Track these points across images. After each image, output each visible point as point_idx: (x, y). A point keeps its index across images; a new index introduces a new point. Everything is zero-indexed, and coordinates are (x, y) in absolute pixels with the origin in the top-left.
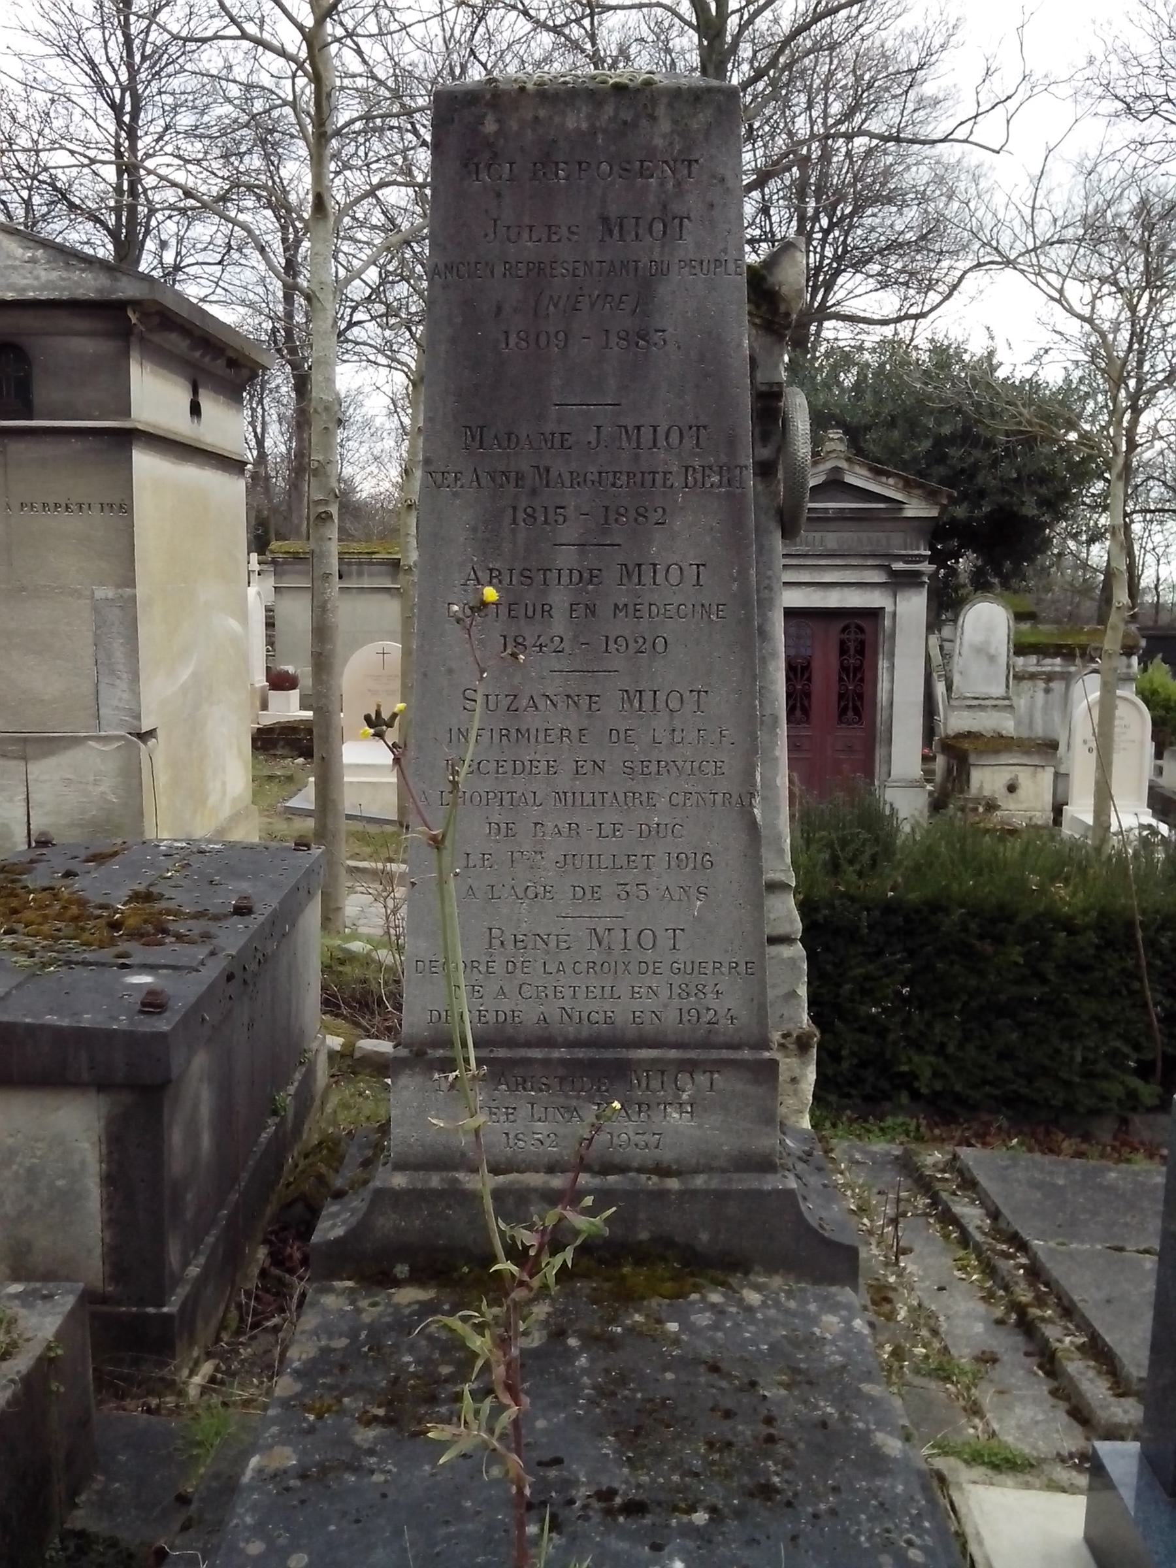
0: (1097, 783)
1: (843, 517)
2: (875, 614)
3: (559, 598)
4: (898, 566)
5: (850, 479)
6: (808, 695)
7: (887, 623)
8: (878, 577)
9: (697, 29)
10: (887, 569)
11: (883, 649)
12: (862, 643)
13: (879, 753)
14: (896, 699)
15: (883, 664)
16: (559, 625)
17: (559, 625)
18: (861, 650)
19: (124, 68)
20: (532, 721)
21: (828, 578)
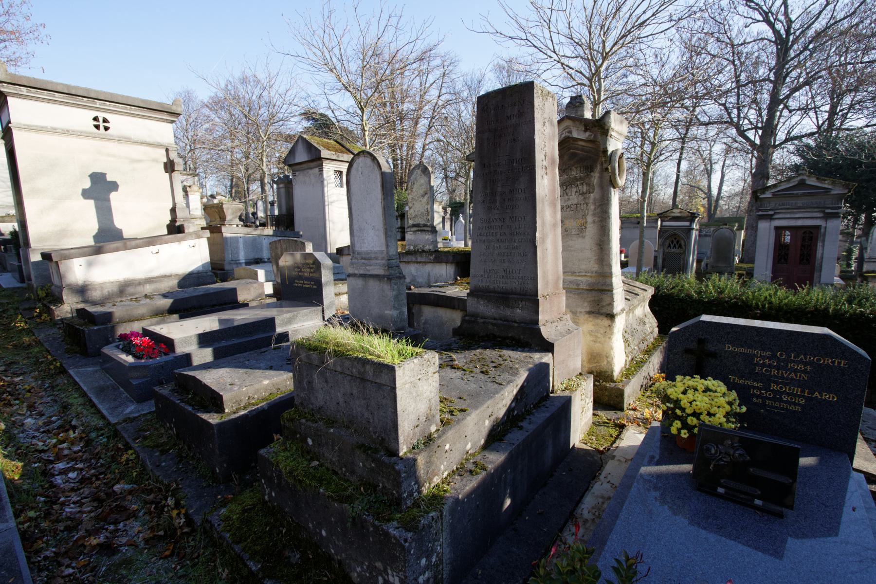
0: (46, 127)
1: (804, 195)
2: (818, 227)
3: (498, 198)
4: (827, 211)
5: (808, 182)
6: (787, 255)
7: (822, 230)
8: (821, 215)
9: (775, 42)
10: (824, 212)
11: (820, 239)
12: (812, 237)
13: (816, 275)
14: (825, 256)
15: (819, 244)
16: (498, 204)
17: (498, 204)
18: (811, 239)
19: (824, 23)
20: (493, 224)
21: (797, 216)
